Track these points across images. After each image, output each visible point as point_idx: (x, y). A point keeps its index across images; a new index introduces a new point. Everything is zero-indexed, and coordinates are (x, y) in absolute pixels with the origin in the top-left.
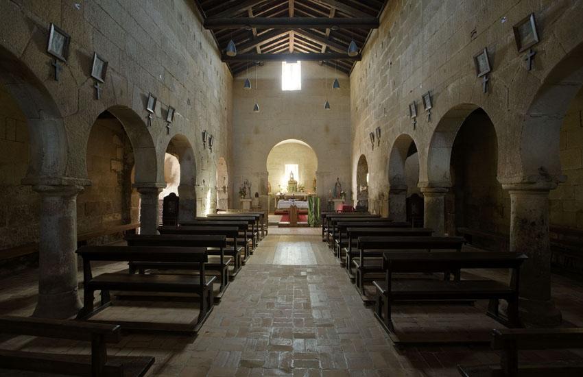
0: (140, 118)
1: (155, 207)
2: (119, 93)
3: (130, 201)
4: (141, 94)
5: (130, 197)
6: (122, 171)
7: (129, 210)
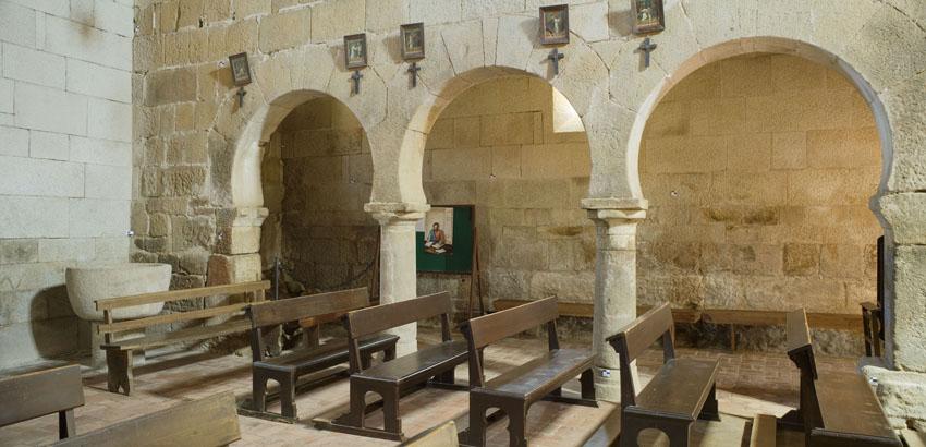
0: (268, 115)
2: (462, 51)
4: (522, 24)
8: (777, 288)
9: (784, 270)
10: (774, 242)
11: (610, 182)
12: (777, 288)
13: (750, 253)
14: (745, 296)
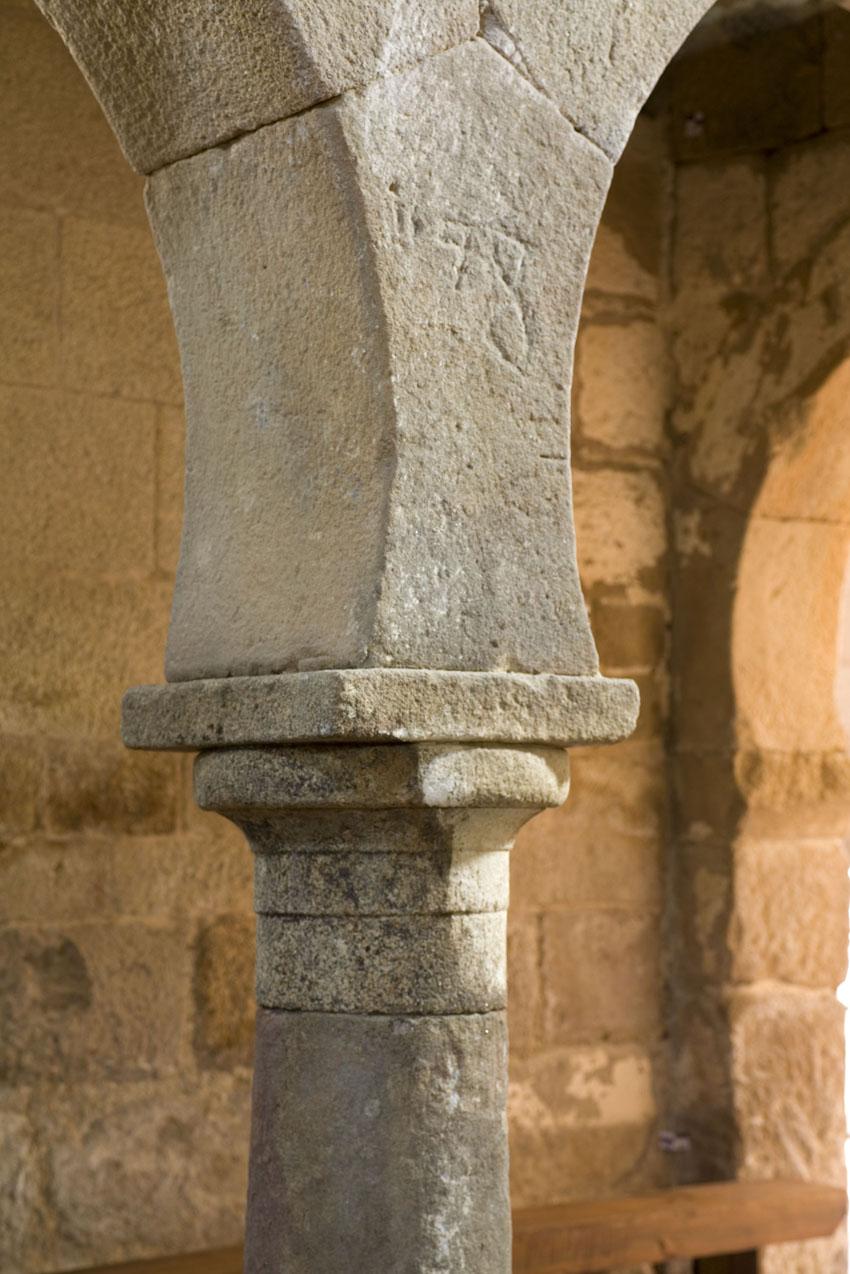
1: (407, 1055)
3: (725, 917)
5: (726, 864)
6: (645, 578)
7: (723, 1016)
8: (177, 1132)
9: (197, 1044)
10: (160, 919)
11: (486, 566)
12: (177, 1132)
13: (65, 964)
14: (48, 1193)
